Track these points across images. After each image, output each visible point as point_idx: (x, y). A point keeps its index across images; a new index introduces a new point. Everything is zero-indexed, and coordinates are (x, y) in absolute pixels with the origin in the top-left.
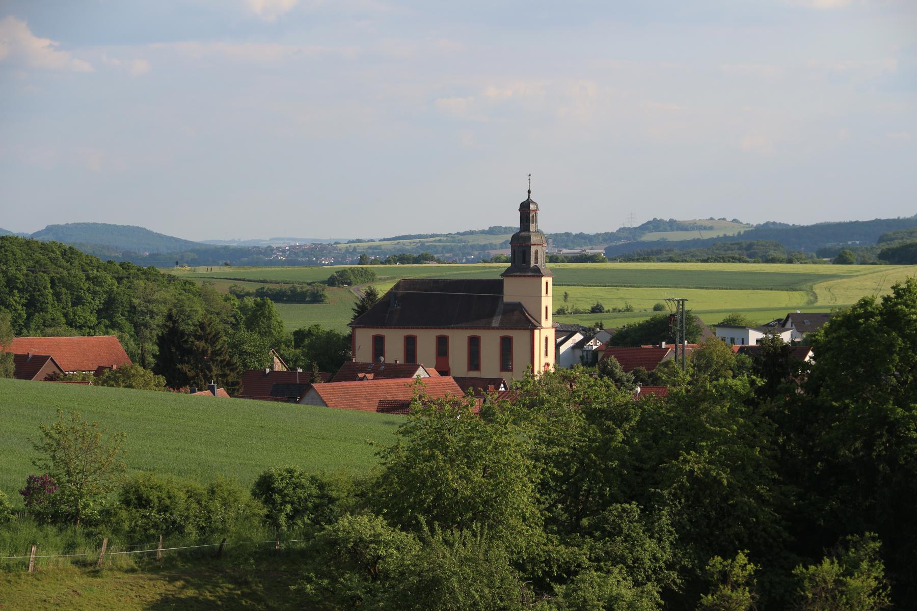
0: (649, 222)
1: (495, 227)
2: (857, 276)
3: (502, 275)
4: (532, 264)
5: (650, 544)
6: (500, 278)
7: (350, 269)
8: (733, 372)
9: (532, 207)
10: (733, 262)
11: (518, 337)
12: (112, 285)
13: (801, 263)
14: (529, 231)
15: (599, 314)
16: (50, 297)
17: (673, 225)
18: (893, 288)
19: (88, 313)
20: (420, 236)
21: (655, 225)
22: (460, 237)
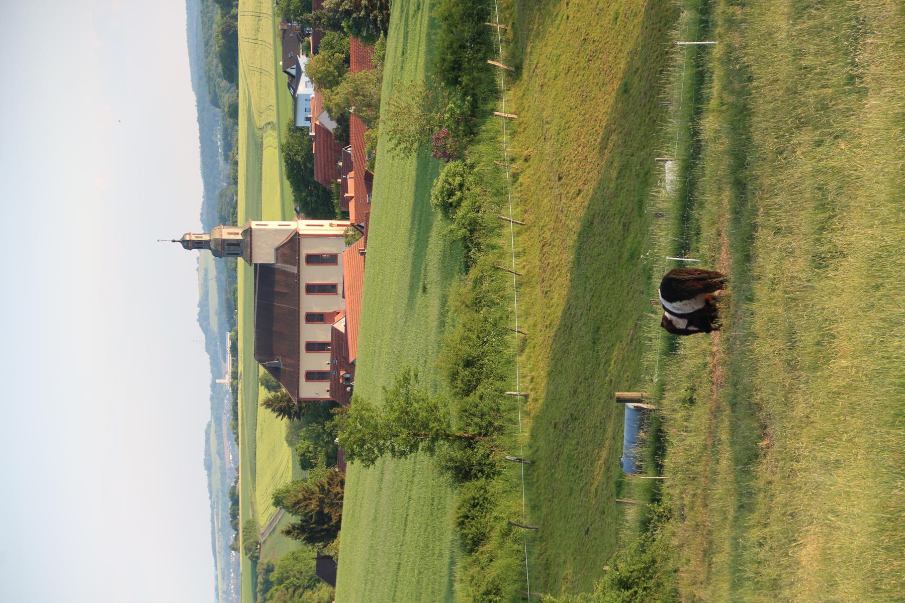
0: (201, 325)
1: (205, 465)
2: (249, 91)
3: (251, 265)
4: (240, 237)
6: (253, 267)
7: (243, 543)
8: (336, 52)
9: (187, 238)
10: (237, 213)
11: (306, 249)
13: (237, 154)
14: (210, 240)
17: (203, 304)
20: (213, 533)
21: (203, 320)
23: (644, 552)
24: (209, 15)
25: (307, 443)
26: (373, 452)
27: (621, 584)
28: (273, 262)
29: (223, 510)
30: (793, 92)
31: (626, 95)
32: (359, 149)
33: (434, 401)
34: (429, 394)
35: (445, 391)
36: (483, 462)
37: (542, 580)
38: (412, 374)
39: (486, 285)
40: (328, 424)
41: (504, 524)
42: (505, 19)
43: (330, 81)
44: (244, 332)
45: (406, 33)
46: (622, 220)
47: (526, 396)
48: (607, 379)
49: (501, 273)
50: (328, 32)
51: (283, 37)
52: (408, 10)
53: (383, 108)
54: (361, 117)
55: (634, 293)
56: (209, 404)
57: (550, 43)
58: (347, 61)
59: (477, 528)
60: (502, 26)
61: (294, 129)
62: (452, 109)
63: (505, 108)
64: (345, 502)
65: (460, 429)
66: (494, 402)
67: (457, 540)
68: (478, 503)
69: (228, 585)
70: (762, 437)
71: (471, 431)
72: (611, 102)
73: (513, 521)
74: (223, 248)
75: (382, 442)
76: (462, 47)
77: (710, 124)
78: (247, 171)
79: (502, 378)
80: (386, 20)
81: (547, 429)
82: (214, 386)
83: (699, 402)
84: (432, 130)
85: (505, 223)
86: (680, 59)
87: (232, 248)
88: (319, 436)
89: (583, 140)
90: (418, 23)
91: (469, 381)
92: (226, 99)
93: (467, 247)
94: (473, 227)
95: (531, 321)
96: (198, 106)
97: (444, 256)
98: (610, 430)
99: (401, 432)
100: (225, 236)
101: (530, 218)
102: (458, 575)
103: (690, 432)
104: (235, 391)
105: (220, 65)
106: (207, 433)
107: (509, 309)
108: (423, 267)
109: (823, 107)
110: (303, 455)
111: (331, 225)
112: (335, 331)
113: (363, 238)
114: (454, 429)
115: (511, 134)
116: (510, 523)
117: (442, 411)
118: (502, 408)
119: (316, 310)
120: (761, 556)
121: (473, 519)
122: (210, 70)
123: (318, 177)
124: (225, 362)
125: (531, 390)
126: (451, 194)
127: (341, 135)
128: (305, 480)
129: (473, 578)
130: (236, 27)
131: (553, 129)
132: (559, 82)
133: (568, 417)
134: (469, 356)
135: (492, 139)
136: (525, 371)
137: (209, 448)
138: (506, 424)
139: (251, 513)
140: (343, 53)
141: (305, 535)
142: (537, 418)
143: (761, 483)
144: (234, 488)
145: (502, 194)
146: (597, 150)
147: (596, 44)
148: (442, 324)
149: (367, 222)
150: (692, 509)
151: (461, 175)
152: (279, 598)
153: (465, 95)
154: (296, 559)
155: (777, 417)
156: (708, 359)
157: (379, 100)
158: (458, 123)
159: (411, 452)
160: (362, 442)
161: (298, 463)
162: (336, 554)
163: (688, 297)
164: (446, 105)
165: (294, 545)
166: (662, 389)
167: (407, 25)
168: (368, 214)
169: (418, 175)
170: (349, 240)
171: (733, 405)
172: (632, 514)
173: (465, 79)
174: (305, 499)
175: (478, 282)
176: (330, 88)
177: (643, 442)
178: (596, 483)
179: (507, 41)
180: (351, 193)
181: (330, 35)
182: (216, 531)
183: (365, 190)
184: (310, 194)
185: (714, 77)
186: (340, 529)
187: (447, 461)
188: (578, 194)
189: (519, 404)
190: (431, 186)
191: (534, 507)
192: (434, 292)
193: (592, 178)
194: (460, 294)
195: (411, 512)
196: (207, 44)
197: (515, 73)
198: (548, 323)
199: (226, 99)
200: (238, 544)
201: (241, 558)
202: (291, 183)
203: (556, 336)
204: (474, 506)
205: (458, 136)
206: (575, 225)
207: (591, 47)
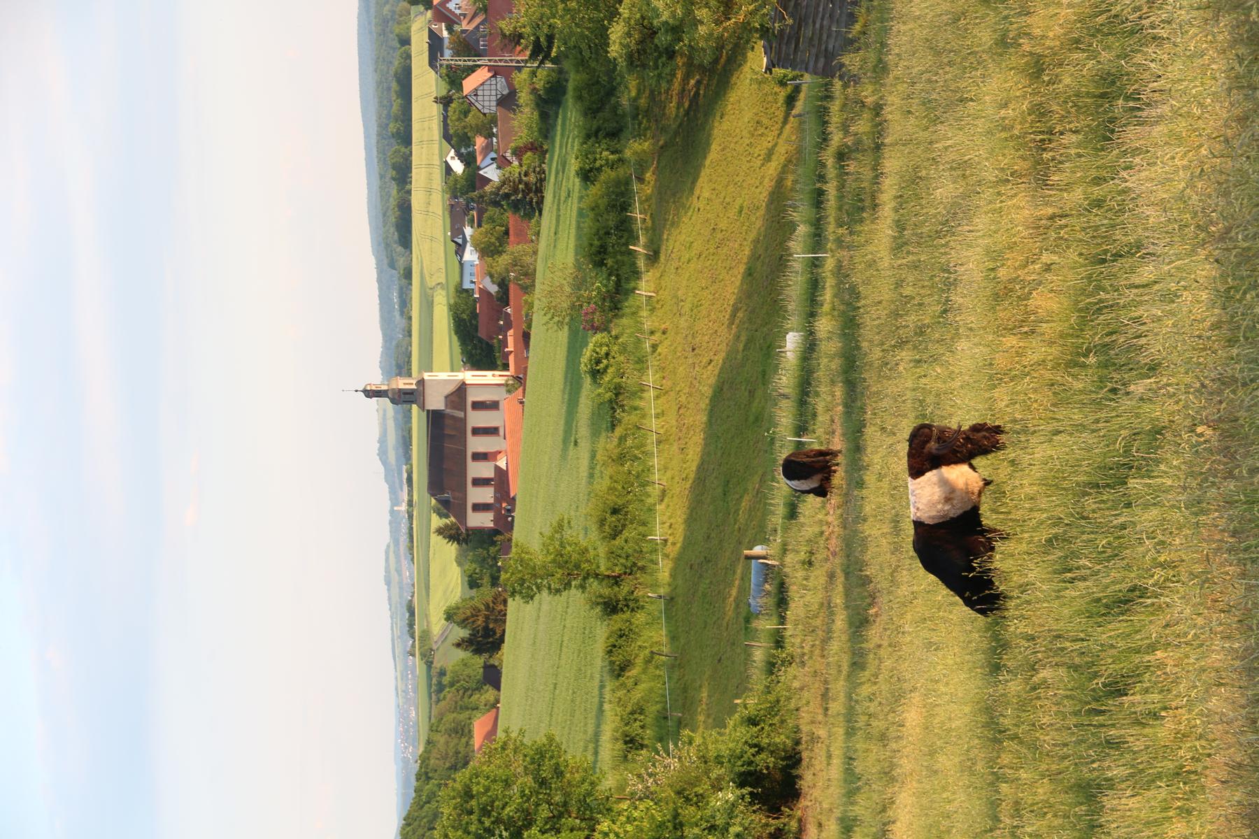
0: (380, 459)
3: (423, 410)
4: (414, 387)
6: (425, 412)
9: (368, 388)
11: (472, 397)
12: (433, 784)
17: (382, 441)
20: (393, 640)
21: (382, 454)
22: (393, 609)
23: (770, 693)
24: (386, 190)
25: (474, 566)
26: (532, 590)
27: (749, 721)
28: (443, 408)
29: (401, 620)
30: (896, 315)
31: (749, 278)
32: (518, 310)
33: (585, 545)
34: (581, 536)
35: (594, 535)
36: (628, 598)
37: (680, 702)
38: (566, 521)
39: (629, 442)
40: (492, 550)
41: (647, 652)
42: (645, 210)
43: (492, 251)
44: (419, 465)
45: (558, 217)
46: (748, 388)
47: (666, 541)
48: (736, 526)
49: (642, 431)
50: (490, 208)
51: (451, 212)
52: (559, 196)
53: (539, 275)
54: (519, 285)
55: (759, 451)
56: (388, 528)
57: (684, 231)
58: (507, 233)
59: (623, 656)
60: (642, 216)
61: (461, 291)
62: (598, 288)
63: (645, 288)
64: (508, 617)
65: (608, 569)
66: (638, 545)
67: (605, 666)
68: (624, 634)
69: (406, 685)
70: (871, 605)
71: (618, 571)
72: (738, 283)
73: (655, 649)
74: (399, 396)
75: (539, 581)
76: (608, 233)
77: (824, 325)
78: (420, 325)
79: (644, 524)
80: (541, 202)
81: (685, 570)
82: (392, 512)
83: (817, 565)
84: (581, 306)
85: (646, 388)
86: (797, 266)
87: (407, 396)
88: (484, 560)
89: (713, 316)
90: (569, 208)
91: (616, 526)
92: (401, 262)
93: (613, 408)
94: (618, 391)
95: (669, 474)
96: (377, 268)
97: (593, 414)
98: (739, 571)
99: (556, 572)
100: (401, 386)
101: (667, 384)
102: (607, 696)
103: (809, 590)
104: (411, 517)
105: (396, 233)
106: (387, 553)
107: (651, 464)
108: (575, 423)
109: (920, 331)
110: (470, 576)
111: (493, 375)
112: (497, 469)
113: (521, 388)
114: (602, 569)
115: (650, 310)
116: (652, 652)
117: (592, 552)
118: (644, 550)
119: (481, 449)
120: (872, 710)
121: (620, 648)
122: (387, 237)
123: (482, 334)
124: (402, 490)
125: (670, 535)
126: (598, 362)
127: (502, 297)
128: (472, 598)
129: (620, 699)
130: (409, 201)
131: (687, 306)
132: (692, 265)
133: (703, 559)
134: (616, 504)
135: (633, 313)
136: (665, 518)
137: (389, 565)
138: (649, 564)
139: (425, 624)
140: (503, 226)
141: (474, 647)
142: (677, 560)
143: (871, 646)
144: (411, 601)
145: (643, 362)
146: (725, 325)
147: (724, 233)
148: (591, 476)
149: (525, 374)
150: (811, 658)
151: (607, 346)
152: (451, 699)
153: (610, 275)
154: (465, 665)
155: (885, 592)
156: (824, 528)
157: (535, 270)
158: (604, 300)
159: (565, 589)
160: (522, 581)
161: (466, 584)
162: (501, 664)
163: (805, 478)
164: (593, 284)
165: (461, 654)
166: (784, 550)
167: (558, 210)
168: (526, 368)
169: (569, 343)
170: (509, 389)
171: (847, 574)
172: (759, 655)
173: (610, 262)
174: (473, 616)
175: (622, 439)
176: (492, 256)
177: (768, 593)
178: (727, 618)
179: (646, 229)
180: (510, 348)
181: (492, 211)
183: (523, 346)
184: (475, 347)
185: (828, 284)
186: (503, 642)
187: (597, 597)
188: (709, 364)
189: (659, 547)
190: (581, 355)
191: (673, 638)
192: (585, 445)
193: (721, 350)
194: (607, 450)
195: (566, 638)
196: (384, 215)
197: (654, 257)
198: (684, 476)
199: (401, 262)
200: (414, 651)
201: (417, 662)
202: (459, 338)
203: (691, 488)
204: (621, 636)
205: (604, 311)
206: (707, 391)
207: (719, 236)
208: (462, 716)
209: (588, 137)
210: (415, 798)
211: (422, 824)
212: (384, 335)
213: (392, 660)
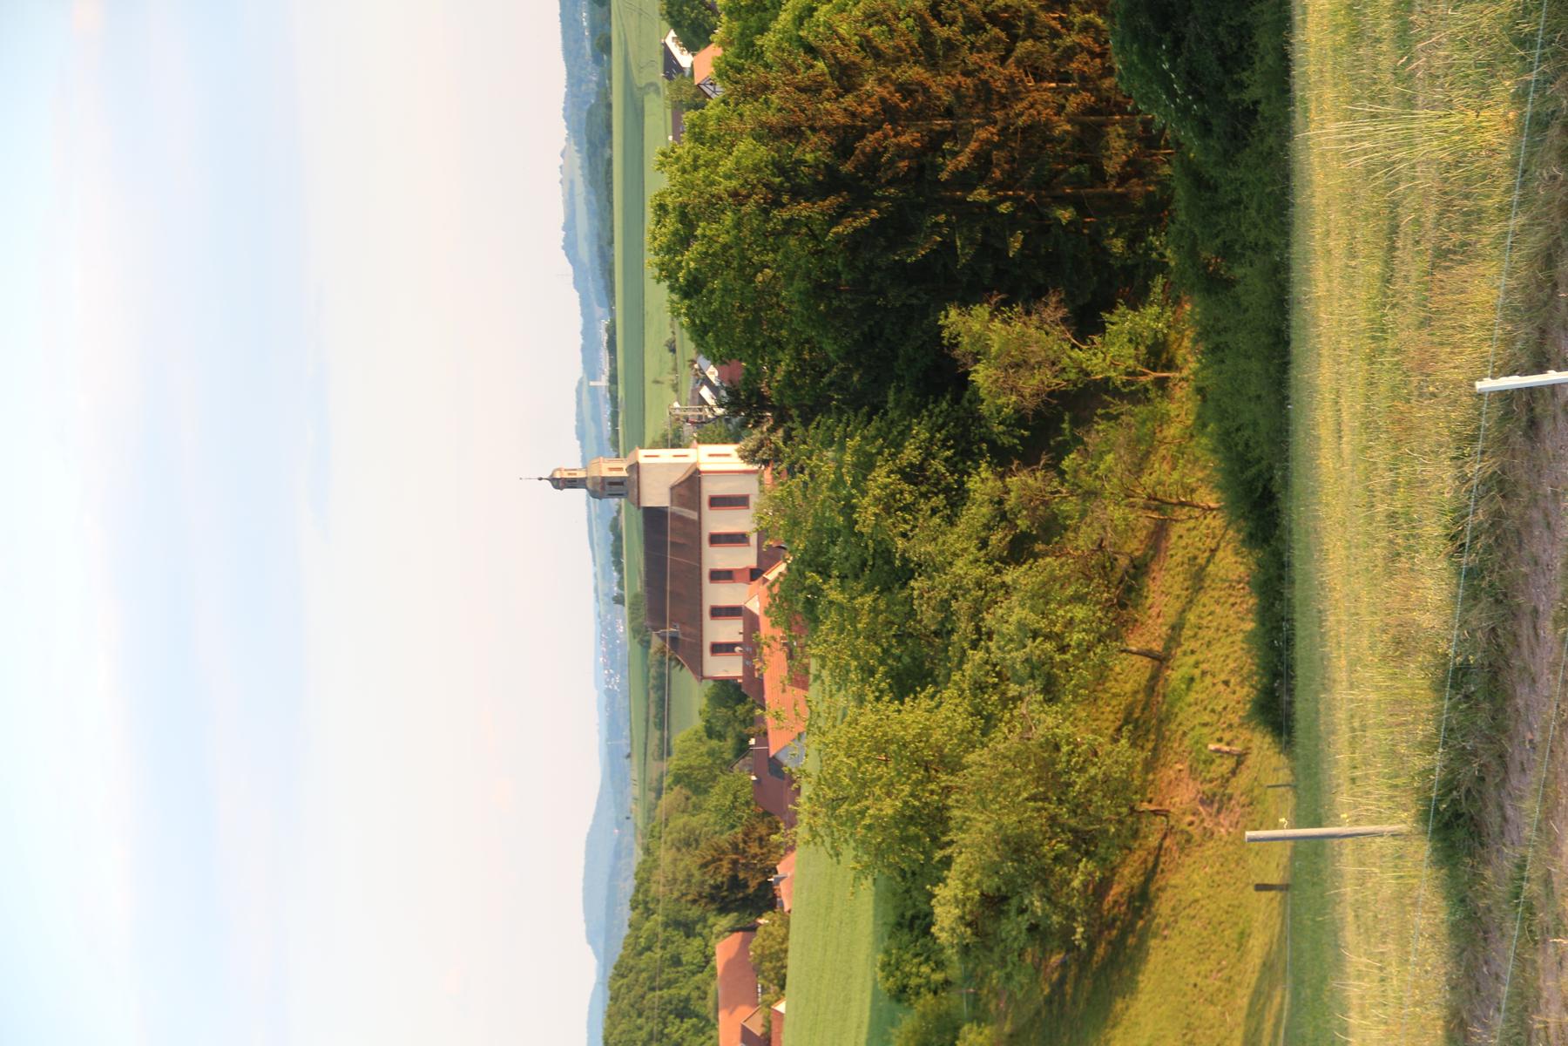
0: (567, 255)
4: (624, 474)
5: (960, 566)
9: (558, 476)
11: (710, 488)
15: (678, 344)
16: (673, 991)
17: (569, 226)
18: (658, 282)
19: (689, 947)
21: (570, 247)
56: (579, 355)
74: (603, 488)
106: (579, 392)
182: (593, 517)
208: (695, 819)
209: (899, 925)
210: (629, 936)
211: (641, 979)
212: (570, 75)
213: (589, 551)
